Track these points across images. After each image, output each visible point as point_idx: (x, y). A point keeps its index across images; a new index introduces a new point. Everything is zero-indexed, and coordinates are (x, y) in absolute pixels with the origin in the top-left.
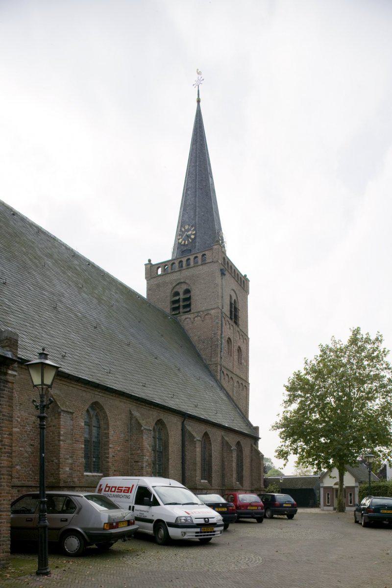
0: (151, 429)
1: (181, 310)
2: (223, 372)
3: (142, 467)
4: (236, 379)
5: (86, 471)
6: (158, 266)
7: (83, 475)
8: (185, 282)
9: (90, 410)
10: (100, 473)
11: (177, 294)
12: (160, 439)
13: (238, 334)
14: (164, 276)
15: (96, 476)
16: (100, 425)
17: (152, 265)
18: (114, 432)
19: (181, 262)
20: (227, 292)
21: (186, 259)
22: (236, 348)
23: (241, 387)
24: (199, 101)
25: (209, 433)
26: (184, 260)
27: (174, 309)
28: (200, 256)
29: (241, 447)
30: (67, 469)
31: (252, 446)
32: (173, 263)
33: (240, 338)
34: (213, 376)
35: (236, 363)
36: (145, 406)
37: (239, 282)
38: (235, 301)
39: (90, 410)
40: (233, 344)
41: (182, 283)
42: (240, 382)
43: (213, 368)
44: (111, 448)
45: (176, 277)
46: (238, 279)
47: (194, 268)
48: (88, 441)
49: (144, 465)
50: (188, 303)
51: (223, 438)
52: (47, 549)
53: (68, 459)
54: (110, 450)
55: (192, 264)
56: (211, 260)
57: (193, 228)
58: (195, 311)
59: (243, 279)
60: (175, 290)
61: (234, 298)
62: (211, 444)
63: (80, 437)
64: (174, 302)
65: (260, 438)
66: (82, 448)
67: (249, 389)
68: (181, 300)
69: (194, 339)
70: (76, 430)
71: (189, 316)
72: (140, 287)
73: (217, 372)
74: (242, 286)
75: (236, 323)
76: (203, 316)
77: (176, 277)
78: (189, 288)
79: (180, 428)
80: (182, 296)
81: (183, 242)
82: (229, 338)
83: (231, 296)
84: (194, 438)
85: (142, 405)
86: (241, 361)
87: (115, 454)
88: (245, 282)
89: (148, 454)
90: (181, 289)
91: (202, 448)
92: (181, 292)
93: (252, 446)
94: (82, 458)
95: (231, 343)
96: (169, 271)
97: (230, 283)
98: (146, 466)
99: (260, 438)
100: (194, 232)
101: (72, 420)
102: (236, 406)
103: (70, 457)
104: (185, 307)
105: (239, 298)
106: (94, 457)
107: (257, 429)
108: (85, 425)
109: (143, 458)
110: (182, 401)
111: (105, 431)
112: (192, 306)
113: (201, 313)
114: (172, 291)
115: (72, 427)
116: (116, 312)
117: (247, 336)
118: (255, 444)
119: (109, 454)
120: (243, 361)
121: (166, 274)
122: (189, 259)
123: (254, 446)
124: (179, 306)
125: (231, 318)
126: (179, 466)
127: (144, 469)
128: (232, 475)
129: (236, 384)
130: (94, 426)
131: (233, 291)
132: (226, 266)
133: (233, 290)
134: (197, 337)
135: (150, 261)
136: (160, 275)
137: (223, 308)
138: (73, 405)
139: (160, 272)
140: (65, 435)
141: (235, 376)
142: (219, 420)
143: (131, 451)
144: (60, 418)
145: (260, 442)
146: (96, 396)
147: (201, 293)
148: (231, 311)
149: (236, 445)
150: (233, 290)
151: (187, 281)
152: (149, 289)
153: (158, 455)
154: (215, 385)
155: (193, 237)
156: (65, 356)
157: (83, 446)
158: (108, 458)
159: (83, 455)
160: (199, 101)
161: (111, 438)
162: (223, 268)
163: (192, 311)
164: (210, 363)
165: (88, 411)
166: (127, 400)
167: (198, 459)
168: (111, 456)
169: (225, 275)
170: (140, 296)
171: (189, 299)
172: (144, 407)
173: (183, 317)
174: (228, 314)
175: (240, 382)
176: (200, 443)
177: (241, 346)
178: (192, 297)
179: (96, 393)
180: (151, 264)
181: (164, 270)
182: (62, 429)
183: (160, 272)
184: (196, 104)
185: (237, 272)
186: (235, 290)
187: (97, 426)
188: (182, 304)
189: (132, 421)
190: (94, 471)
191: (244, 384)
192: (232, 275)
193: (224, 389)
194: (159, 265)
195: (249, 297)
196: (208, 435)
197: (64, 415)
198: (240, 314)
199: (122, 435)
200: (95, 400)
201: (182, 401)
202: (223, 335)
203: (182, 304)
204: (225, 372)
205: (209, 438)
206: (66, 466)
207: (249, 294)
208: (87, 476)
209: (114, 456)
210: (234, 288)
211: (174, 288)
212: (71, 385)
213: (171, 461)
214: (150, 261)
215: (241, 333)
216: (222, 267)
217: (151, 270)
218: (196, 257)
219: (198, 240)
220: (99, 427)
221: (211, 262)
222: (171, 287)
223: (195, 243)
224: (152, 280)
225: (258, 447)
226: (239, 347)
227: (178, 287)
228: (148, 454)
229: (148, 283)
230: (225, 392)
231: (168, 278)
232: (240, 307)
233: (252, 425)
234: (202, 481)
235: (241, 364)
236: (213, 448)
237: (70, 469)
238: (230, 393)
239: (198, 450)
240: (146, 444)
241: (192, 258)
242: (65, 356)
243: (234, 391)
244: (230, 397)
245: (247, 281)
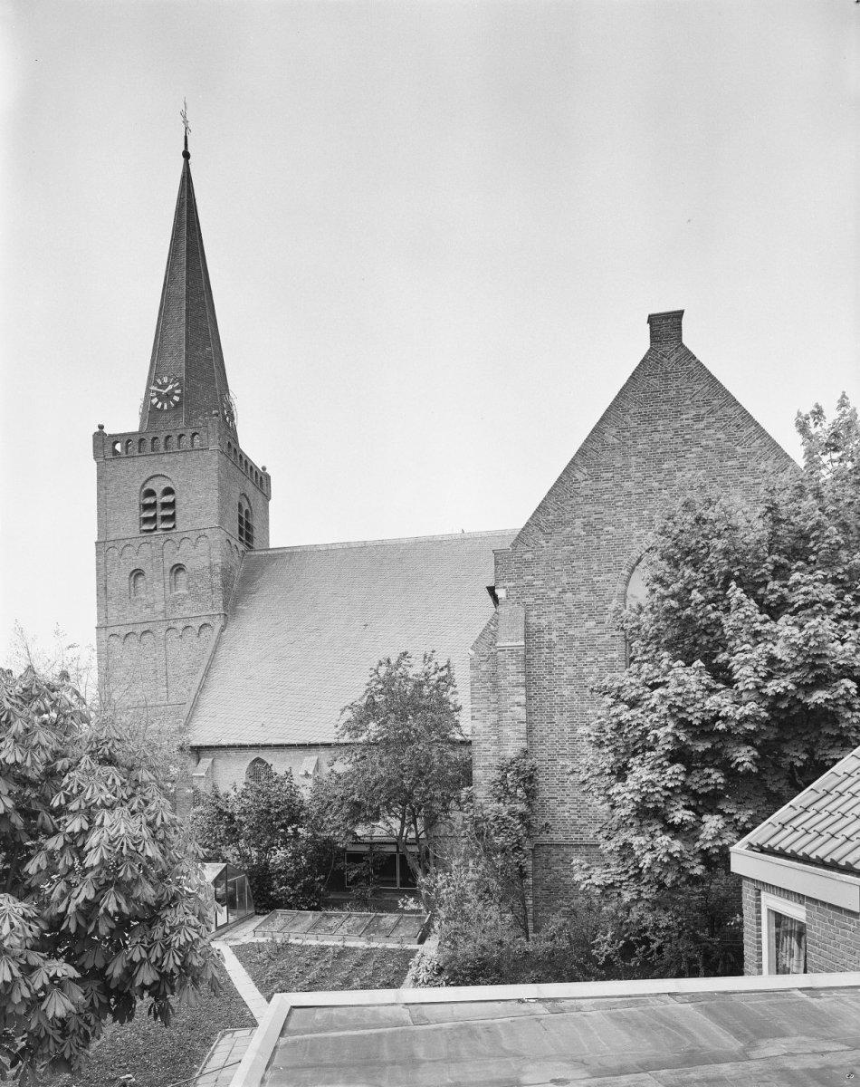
6: (115, 439)
11: (150, 493)
24: (186, 155)
50: (171, 513)
52: (355, 1033)
60: (149, 486)
61: (245, 507)
68: (159, 505)
81: (160, 404)
92: (159, 489)
112: (178, 517)
135: (101, 427)
155: (176, 399)
160: (186, 155)
185: (249, 464)
214: (101, 427)
227: (151, 482)
232: (255, 523)
245: (268, 477)
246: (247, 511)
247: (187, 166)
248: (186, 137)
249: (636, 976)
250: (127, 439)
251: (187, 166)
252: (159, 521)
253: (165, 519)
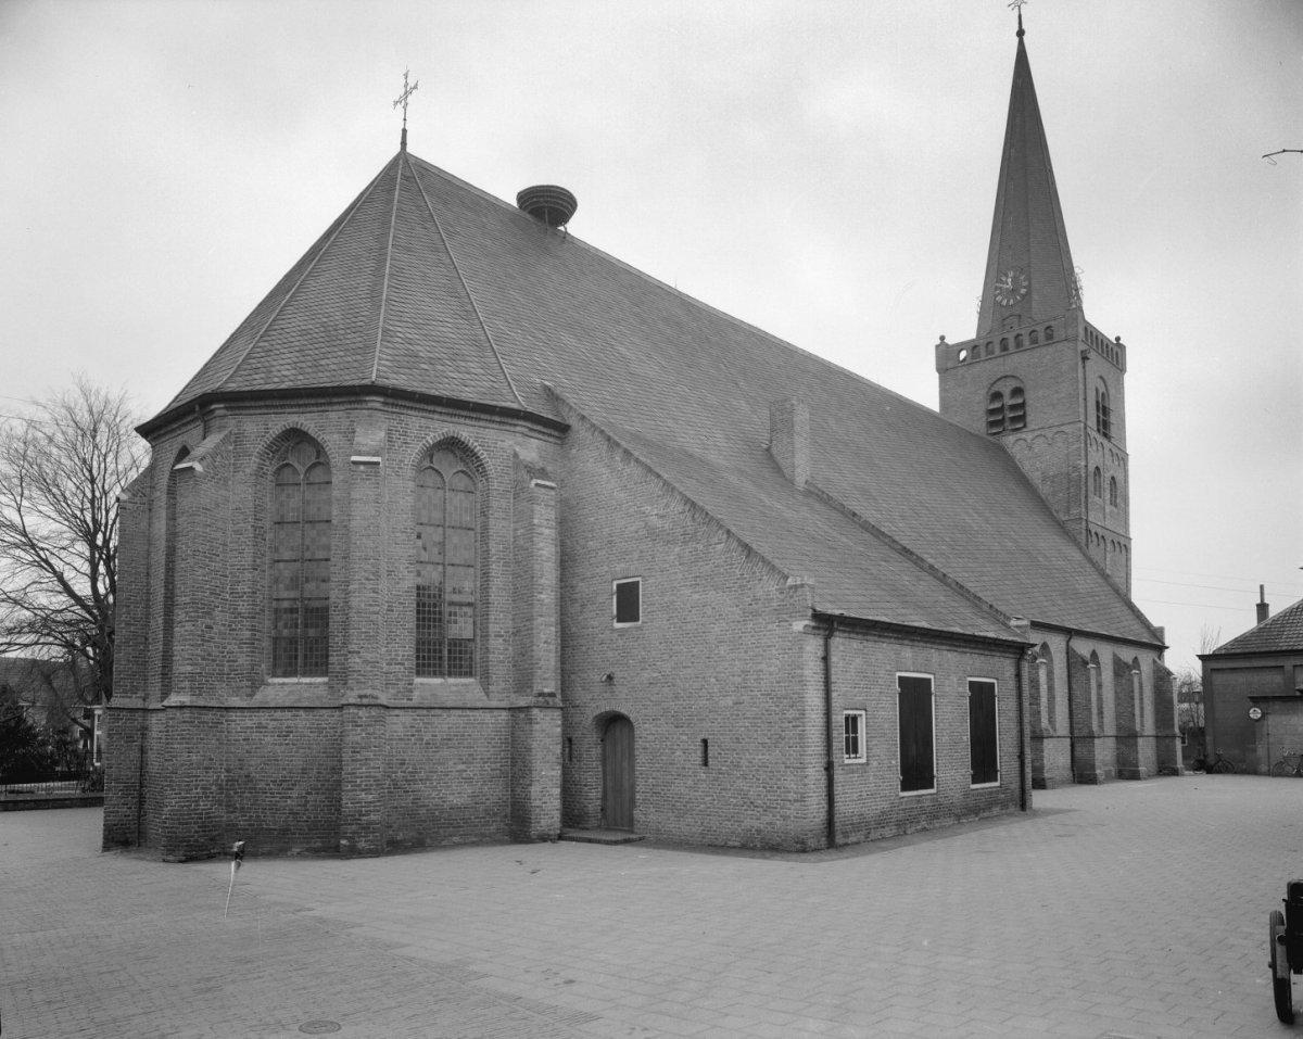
6: (961, 346)
11: (997, 396)
20: (1093, 382)
23: (1117, 549)
24: (1021, 33)
27: (992, 424)
43: (1071, 526)
50: (1020, 401)
55: (1027, 343)
60: (995, 389)
61: (1101, 391)
64: (992, 412)
65: (1167, 648)
69: (1035, 477)
72: (924, 390)
76: (1050, 435)
78: (1022, 386)
82: (1097, 468)
83: (1097, 390)
90: (1006, 388)
92: (1006, 391)
93: (1154, 661)
97: (1096, 364)
99: (1167, 648)
104: (1014, 420)
107: (1161, 630)
112: (1029, 419)
124: (1003, 418)
129: (1109, 545)
133: (1101, 377)
135: (942, 338)
150: (1101, 377)
160: (1021, 33)
163: (1031, 426)
170: (927, 413)
171: (1022, 406)
184: (1016, 40)
185: (1100, 337)
186: (1105, 378)
191: (1122, 543)
195: (1127, 377)
198: (1113, 419)
211: (992, 385)
214: (942, 338)
226: (1113, 478)
245: (1122, 348)
246: (1103, 394)
247: (1021, 44)
248: (1020, 17)
249: (266, 848)
250: (972, 347)
251: (1021, 44)
252: (1007, 424)
253: (1014, 420)
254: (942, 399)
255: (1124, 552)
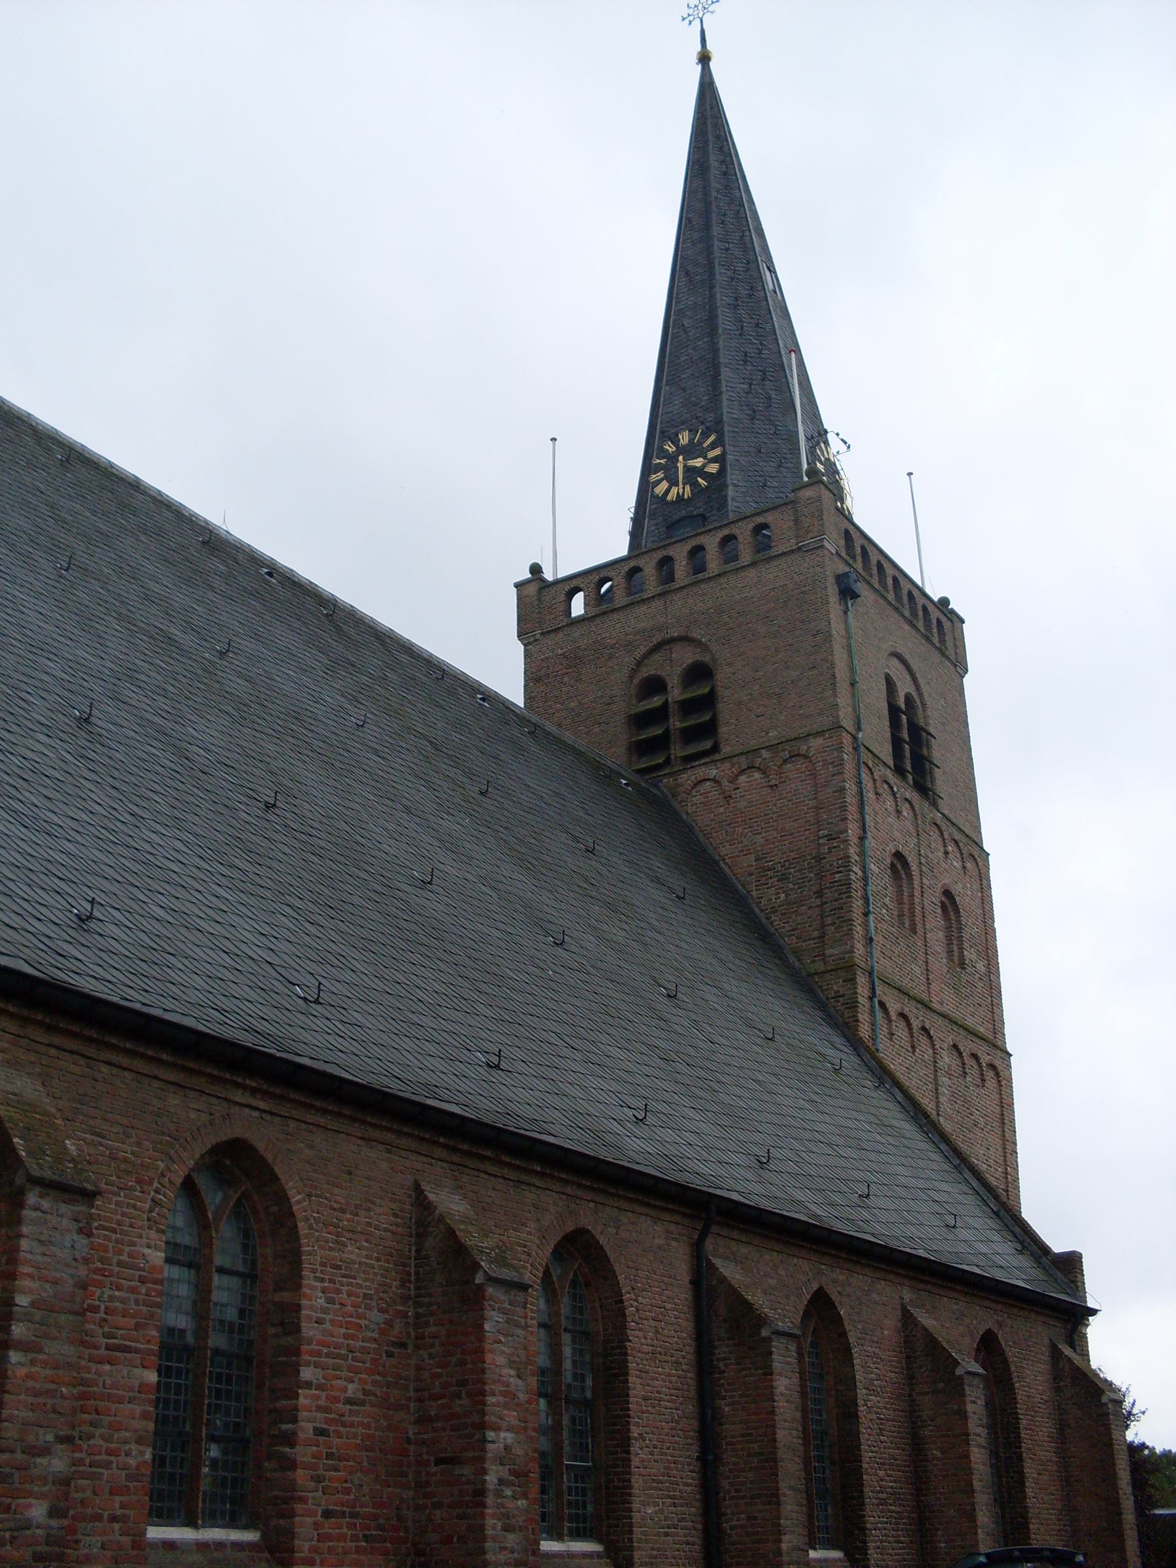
0: (527, 1278)
1: (678, 750)
2: (882, 1005)
3: (481, 1492)
4: (944, 1036)
5: (163, 1516)
6: (572, 585)
7: (139, 1542)
8: (685, 639)
9: (203, 1182)
10: (246, 1527)
11: (655, 685)
12: (582, 1336)
13: (935, 834)
14: (598, 621)
15: (220, 1545)
16: (254, 1262)
17: (545, 585)
18: (330, 1301)
19: (666, 562)
21: (688, 546)
22: (932, 900)
24: (704, 59)
25: (834, 1297)
26: (680, 554)
27: (642, 748)
28: (743, 532)
29: (1005, 1362)
30: (38, 1511)
31: (1055, 1353)
32: (636, 570)
33: (946, 853)
34: (846, 1029)
35: (940, 964)
36: (498, 1162)
37: (920, 625)
38: (908, 699)
39: (203, 1182)
40: (916, 883)
41: (672, 640)
42: (967, 1046)
44: (308, 1385)
45: (646, 618)
46: (914, 614)
47: (723, 580)
48: (186, 1348)
49: (491, 1479)
51: (907, 1319)
53: (45, 1451)
54: (304, 1399)
55: (714, 564)
56: (792, 544)
57: (712, 438)
58: (738, 750)
59: (935, 614)
60: (646, 671)
61: (904, 687)
62: (848, 1349)
63: (138, 1327)
64: (641, 720)
65: (1094, 1312)
66: (143, 1387)
67: (1010, 1080)
68: (673, 708)
70: (119, 1288)
71: (713, 772)
73: (853, 1005)
74: (936, 640)
75: (924, 788)
77: (646, 618)
78: (707, 659)
79: (682, 1269)
80: (676, 693)
82: (964, 968)
83: (889, 682)
84: (761, 1321)
85: (483, 1158)
86: (962, 957)
87: (329, 1421)
88: (947, 625)
89: (512, 1417)
91: (802, 1373)
93: (1055, 1353)
94: (139, 1441)
95: (910, 876)
96: (620, 599)
98: (501, 1482)
99: (1094, 1312)
100: (717, 452)
101: (85, 1231)
102: (960, 1161)
103: (61, 1440)
104: (691, 735)
105: (925, 689)
106: (212, 1438)
107: (1070, 1264)
108: (169, 1261)
109: (484, 1440)
110: (692, 1138)
111: (277, 1298)
112: (723, 730)
113: (765, 754)
114: (631, 678)
115: (83, 1272)
116: (376, 752)
117: (979, 845)
118: (1072, 1346)
119: (294, 1420)
120: (970, 955)
121: (604, 613)
122: (698, 550)
123: (1067, 1351)
124: (667, 732)
125: (899, 770)
126: (687, 1480)
127: (490, 1500)
128: (972, 1516)
129: (947, 1059)
130: (221, 1270)
131: (895, 662)
132: (859, 565)
134: (752, 857)
136: (580, 620)
137: (859, 729)
138: (113, 1157)
139: (578, 606)
140: (38, 1315)
141: (940, 1021)
142: (879, 1228)
143: (419, 1400)
144: (19, 1222)
145: (1096, 1333)
146: (236, 1110)
147: (758, 675)
148: (897, 743)
149: (978, 1350)
151: (696, 634)
152: (533, 678)
153: (573, 1420)
154: (850, 1061)
156: (90, 917)
157: (152, 1377)
158: (290, 1439)
159: (151, 1426)
160: (704, 59)
161: (309, 1330)
162: (847, 569)
163: (726, 750)
164: (820, 967)
165: (189, 1187)
166: (399, 1133)
167: (788, 1434)
168: (306, 1428)
169: (855, 596)
171: (709, 701)
172: (492, 1169)
173: (687, 778)
174: (885, 751)
175: (967, 1046)
176: (793, 1348)
177: (957, 889)
178: (720, 691)
179: (239, 1096)
180: (543, 580)
181: (596, 601)
182: (27, 1283)
183: (578, 606)
186: (907, 657)
187: (241, 1268)
188: (676, 723)
189: (429, 1242)
190: (212, 1520)
191: (985, 1059)
192: (885, 599)
193: (898, 1085)
194: (574, 583)
195: (969, 683)
196: (831, 1305)
197: (45, 1204)
198: (937, 752)
199: (376, 1316)
200: (226, 1134)
201: (692, 1138)
202: (870, 842)
203: (676, 723)
204: (893, 1007)
205: (839, 1320)
206: (30, 1494)
207: (966, 671)
208: (170, 1545)
209: (320, 1432)
210: (901, 650)
211: (639, 664)
212: (106, 1055)
213: (639, 1453)
215: (949, 832)
216: (842, 568)
217: (539, 600)
218: (729, 539)
219: (732, 477)
220: (250, 1277)
221: (792, 552)
222: (629, 660)
223: (724, 486)
224: (550, 641)
225: (1085, 1355)
226: (947, 893)
227: (656, 657)
228: (512, 1417)
229: (527, 655)
230: (899, 1096)
231: (614, 628)
232: (933, 721)
233: (1044, 1249)
234: (812, 1554)
235: (962, 965)
236: (859, 1377)
237: (54, 1512)
238: (927, 1103)
239: (785, 1384)
240: (501, 1360)
241: (711, 542)
242: (90, 917)
243: (942, 1090)
244: (926, 1115)
245: (956, 620)
254: (525, 704)
255: (991, 1083)
